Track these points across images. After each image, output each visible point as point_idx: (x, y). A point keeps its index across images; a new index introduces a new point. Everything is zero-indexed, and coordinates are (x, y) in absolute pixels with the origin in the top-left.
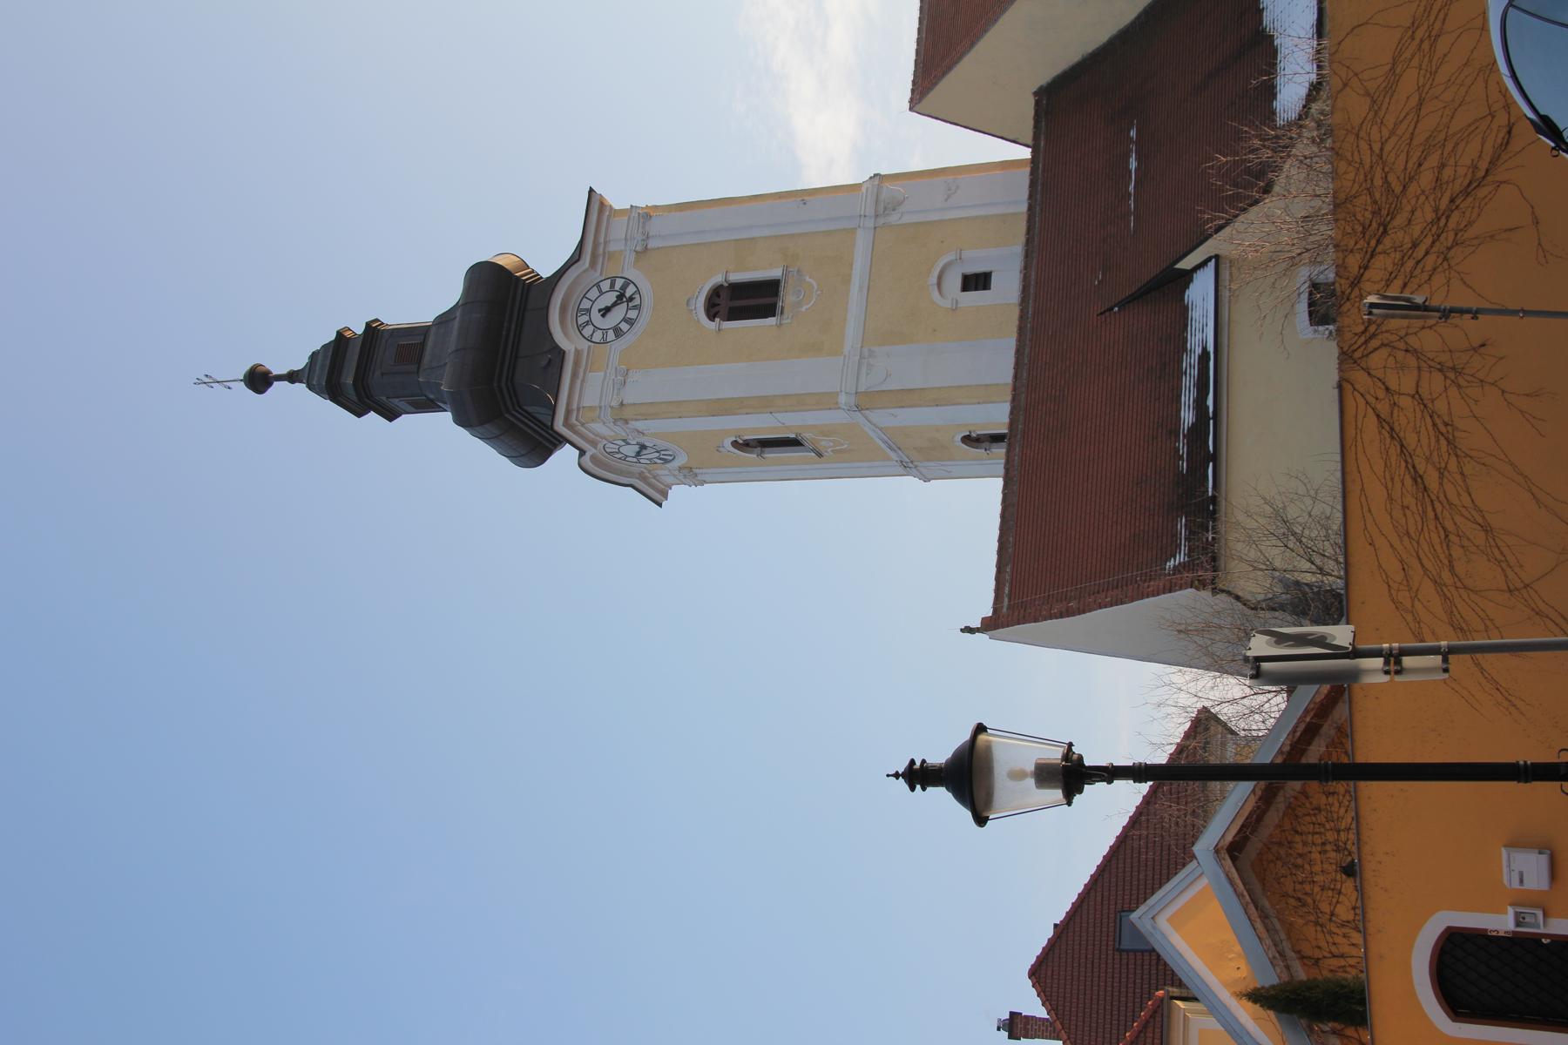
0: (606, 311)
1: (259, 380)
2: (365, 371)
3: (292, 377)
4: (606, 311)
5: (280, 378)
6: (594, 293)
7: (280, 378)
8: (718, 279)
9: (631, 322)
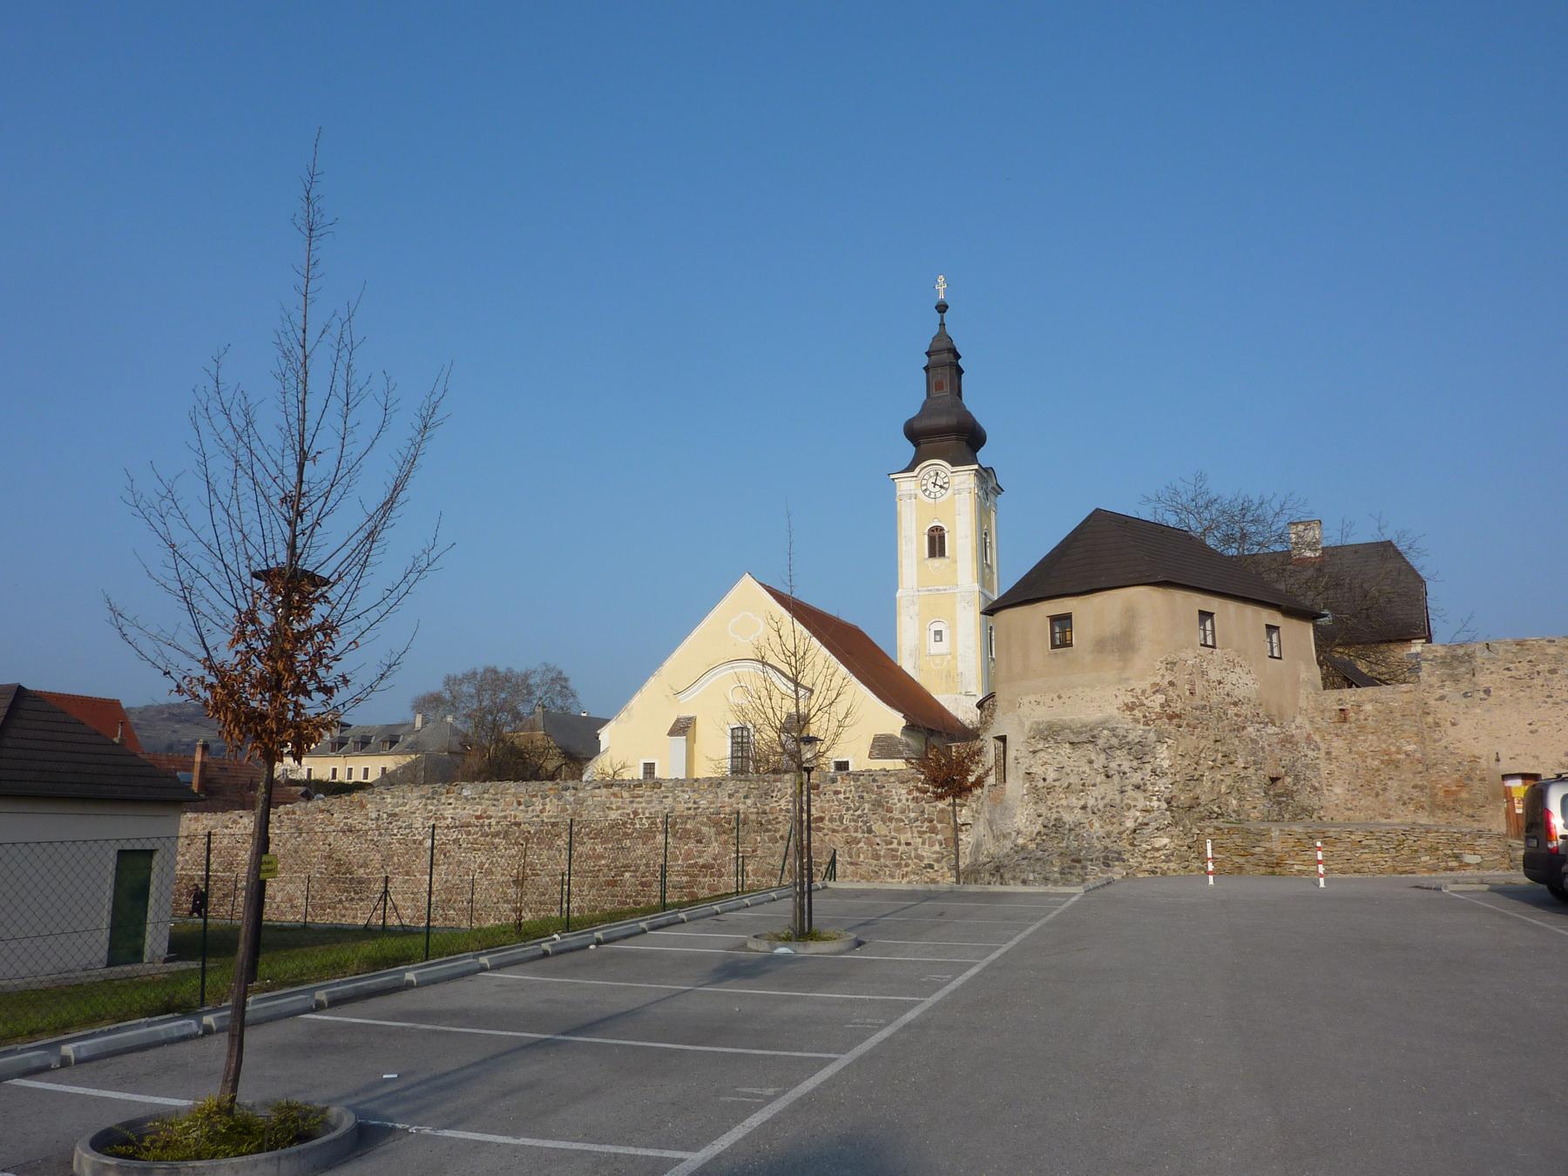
1: (942, 308)
2: (945, 364)
3: (942, 325)
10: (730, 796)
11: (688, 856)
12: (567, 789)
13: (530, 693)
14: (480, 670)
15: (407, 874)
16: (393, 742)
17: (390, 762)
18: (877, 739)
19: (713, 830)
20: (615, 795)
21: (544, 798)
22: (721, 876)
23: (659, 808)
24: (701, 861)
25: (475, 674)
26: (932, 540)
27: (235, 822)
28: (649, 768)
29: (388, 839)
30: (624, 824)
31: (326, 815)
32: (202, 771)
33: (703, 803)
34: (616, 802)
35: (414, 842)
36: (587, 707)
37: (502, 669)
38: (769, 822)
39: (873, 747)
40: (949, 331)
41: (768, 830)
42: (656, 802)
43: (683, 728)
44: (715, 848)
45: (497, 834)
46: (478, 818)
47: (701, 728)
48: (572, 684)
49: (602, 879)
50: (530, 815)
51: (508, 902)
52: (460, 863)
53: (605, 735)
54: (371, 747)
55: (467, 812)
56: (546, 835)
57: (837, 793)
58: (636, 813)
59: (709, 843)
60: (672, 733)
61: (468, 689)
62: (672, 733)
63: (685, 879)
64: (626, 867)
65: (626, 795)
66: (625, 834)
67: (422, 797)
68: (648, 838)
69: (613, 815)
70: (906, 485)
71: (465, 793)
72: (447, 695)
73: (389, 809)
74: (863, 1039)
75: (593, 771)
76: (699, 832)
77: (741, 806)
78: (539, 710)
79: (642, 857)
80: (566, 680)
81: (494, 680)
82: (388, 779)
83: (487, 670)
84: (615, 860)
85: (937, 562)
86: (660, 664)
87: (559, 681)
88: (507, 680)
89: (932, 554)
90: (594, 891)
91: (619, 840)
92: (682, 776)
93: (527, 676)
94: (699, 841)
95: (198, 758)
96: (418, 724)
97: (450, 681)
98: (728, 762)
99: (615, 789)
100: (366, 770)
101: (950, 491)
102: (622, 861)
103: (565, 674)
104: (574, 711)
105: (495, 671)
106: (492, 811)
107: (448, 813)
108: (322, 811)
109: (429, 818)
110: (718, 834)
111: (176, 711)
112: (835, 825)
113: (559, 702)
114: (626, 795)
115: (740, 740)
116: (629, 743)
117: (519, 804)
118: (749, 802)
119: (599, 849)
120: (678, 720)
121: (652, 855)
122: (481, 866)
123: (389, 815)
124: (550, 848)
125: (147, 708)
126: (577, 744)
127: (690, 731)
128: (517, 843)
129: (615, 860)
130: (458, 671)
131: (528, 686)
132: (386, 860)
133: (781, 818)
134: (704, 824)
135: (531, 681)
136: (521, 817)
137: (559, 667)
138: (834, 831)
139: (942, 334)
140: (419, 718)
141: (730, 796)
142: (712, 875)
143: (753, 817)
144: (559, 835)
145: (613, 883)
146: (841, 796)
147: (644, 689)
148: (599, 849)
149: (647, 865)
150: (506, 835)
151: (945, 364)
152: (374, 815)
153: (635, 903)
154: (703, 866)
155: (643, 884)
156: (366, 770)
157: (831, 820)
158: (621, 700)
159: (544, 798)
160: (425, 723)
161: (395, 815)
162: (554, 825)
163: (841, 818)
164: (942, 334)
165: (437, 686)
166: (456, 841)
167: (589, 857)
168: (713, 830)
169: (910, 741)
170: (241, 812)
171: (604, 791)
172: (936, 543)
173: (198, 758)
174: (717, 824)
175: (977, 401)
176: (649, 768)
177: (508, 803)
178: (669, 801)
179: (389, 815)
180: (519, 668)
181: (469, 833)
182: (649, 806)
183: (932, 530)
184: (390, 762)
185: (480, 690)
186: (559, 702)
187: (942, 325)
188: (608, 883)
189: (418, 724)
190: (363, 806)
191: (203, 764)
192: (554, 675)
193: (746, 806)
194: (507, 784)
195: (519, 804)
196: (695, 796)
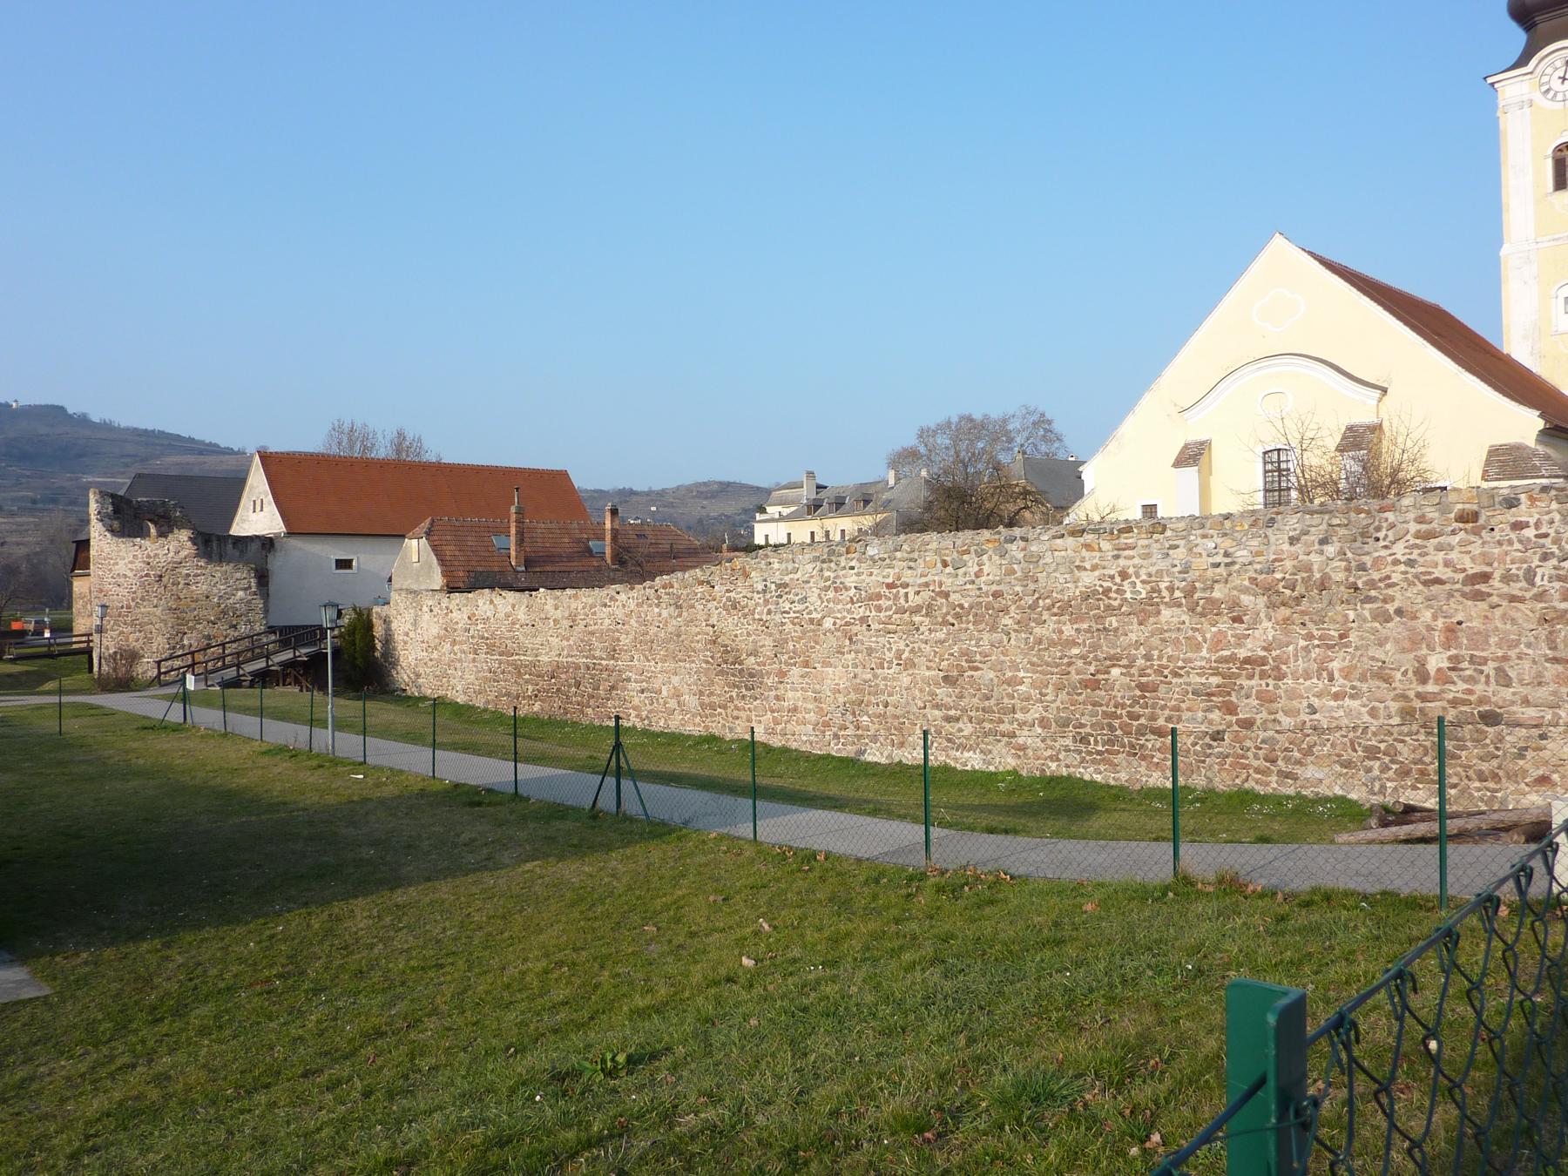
10: (1293, 541)
11: (1217, 644)
12: (1012, 540)
13: (1010, 440)
14: (955, 419)
15: (806, 664)
16: (867, 502)
17: (867, 521)
18: (1494, 452)
19: (1262, 601)
20: (1087, 547)
21: (980, 554)
22: (1280, 677)
23: (1163, 565)
24: (1242, 653)
25: (949, 423)
27: (612, 599)
28: (1149, 510)
29: (778, 618)
30: (1107, 591)
31: (706, 588)
32: (614, 539)
33: (1242, 555)
34: (1090, 558)
35: (811, 621)
36: (1071, 448)
37: (977, 416)
38: (1372, 584)
39: (1488, 463)
41: (1369, 600)
42: (1157, 556)
43: (1192, 455)
44: (1267, 629)
45: (916, 610)
46: (890, 586)
47: (1219, 455)
48: (1056, 427)
49: (1075, 677)
50: (961, 580)
51: (937, 707)
52: (870, 651)
53: (1089, 474)
54: (846, 507)
55: (875, 579)
56: (988, 611)
57: (1518, 526)
58: (1124, 575)
59: (1256, 621)
60: (1178, 463)
61: (943, 440)
62: (1178, 463)
63: (1215, 680)
64: (1114, 660)
65: (1105, 545)
66: (1109, 607)
67: (816, 559)
68: (1148, 615)
69: (1088, 579)
70: (1514, 89)
71: (871, 551)
72: (923, 450)
73: (777, 578)
75: (1078, 514)
76: (1236, 604)
77: (1314, 558)
78: (1020, 457)
79: (1138, 644)
80: (1050, 422)
81: (971, 428)
82: (860, 537)
83: (962, 418)
84: (1095, 647)
86: (1155, 374)
87: (1042, 425)
88: (983, 426)
90: (1063, 696)
91: (1099, 618)
92: (1170, 879)
93: (1005, 421)
94: (1237, 620)
95: (608, 525)
96: (892, 482)
97: (924, 434)
98: (1260, 497)
99: (1088, 538)
100: (812, 534)
102: (1106, 649)
103: (1048, 416)
104: (1061, 456)
105: (970, 419)
106: (907, 576)
107: (851, 580)
108: (701, 583)
109: (827, 589)
110: (1272, 606)
111: (703, 489)
112: (1516, 588)
113: (1043, 448)
114: (1105, 545)
115: (1275, 466)
116: (1118, 480)
117: (945, 564)
118: (1330, 550)
119: (1068, 630)
120: (1186, 447)
121: (1155, 641)
122: (899, 656)
123: (779, 586)
124: (993, 629)
125: (678, 488)
126: (1049, 489)
127: (1204, 459)
128: (945, 623)
129: (1095, 647)
130: (933, 420)
131: (1007, 433)
132: (780, 645)
133: (1396, 578)
134: (1245, 591)
135: (1010, 427)
136: (948, 584)
137: (1041, 409)
138: (1513, 599)
140: (892, 474)
141: (1293, 541)
142: (1263, 675)
143: (1340, 576)
144: (1005, 610)
145: (1094, 684)
146: (1530, 533)
147: (1138, 409)
148: (1068, 630)
149: (1148, 657)
150: (930, 610)
152: (760, 587)
153: (1134, 716)
154: (1247, 661)
155: (1142, 687)
156: (812, 534)
157: (1507, 578)
158: (1102, 434)
159: (980, 554)
160: (898, 479)
161: (785, 585)
162: (997, 595)
163: (1530, 576)
165: (910, 440)
166: (864, 620)
167: (1052, 643)
168: (1262, 601)
169: (1550, 451)
170: (617, 587)
171: (1070, 541)
173: (608, 525)
174: (1268, 589)
176: (1149, 510)
177: (976, 564)
178: (1179, 554)
180: (995, 414)
181: (879, 609)
182: (1147, 563)
184: (867, 521)
185: (956, 440)
186: (1043, 448)
188: (1086, 684)
189: (892, 482)
190: (747, 576)
191: (615, 534)
192: (1035, 418)
193: (1328, 561)
194: (926, 537)
195: (945, 564)
196: (1226, 543)
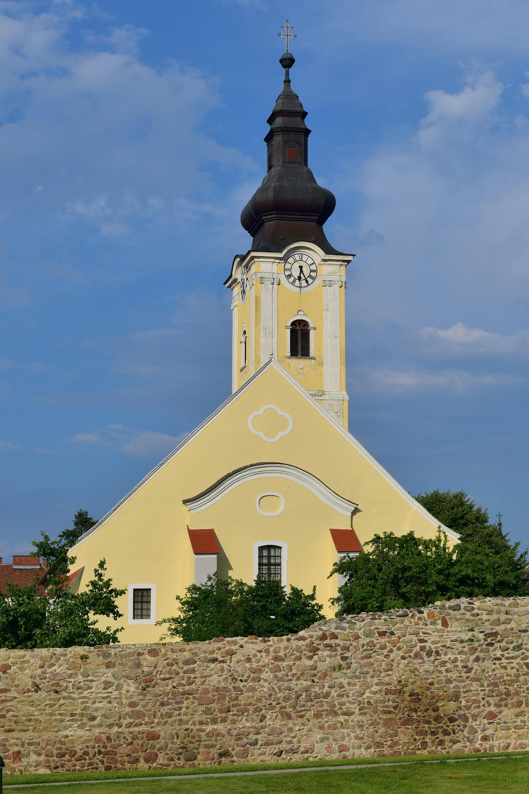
0: (301, 267)
1: (288, 62)
2: (288, 130)
3: (287, 82)
4: (301, 267)
5: (287, 74)
6: (310, 261)
7: (287, 74)
8: (311, 325)
9: (314, 279)
26: (293, 333)
37: (441, 492)
40: (294, 88)
74: (205, 777)
85: (300, 363)
89: (294, 353)
101: (318, 282)
123: (487, 636)
139: (288, 96)
151: (288, 130)
161: (496, 634)
164: (288, 96)
172: (300, 339)
175: (325, 169)
179: (487, 636)
183: (294, 324)
187: (287, 82)
